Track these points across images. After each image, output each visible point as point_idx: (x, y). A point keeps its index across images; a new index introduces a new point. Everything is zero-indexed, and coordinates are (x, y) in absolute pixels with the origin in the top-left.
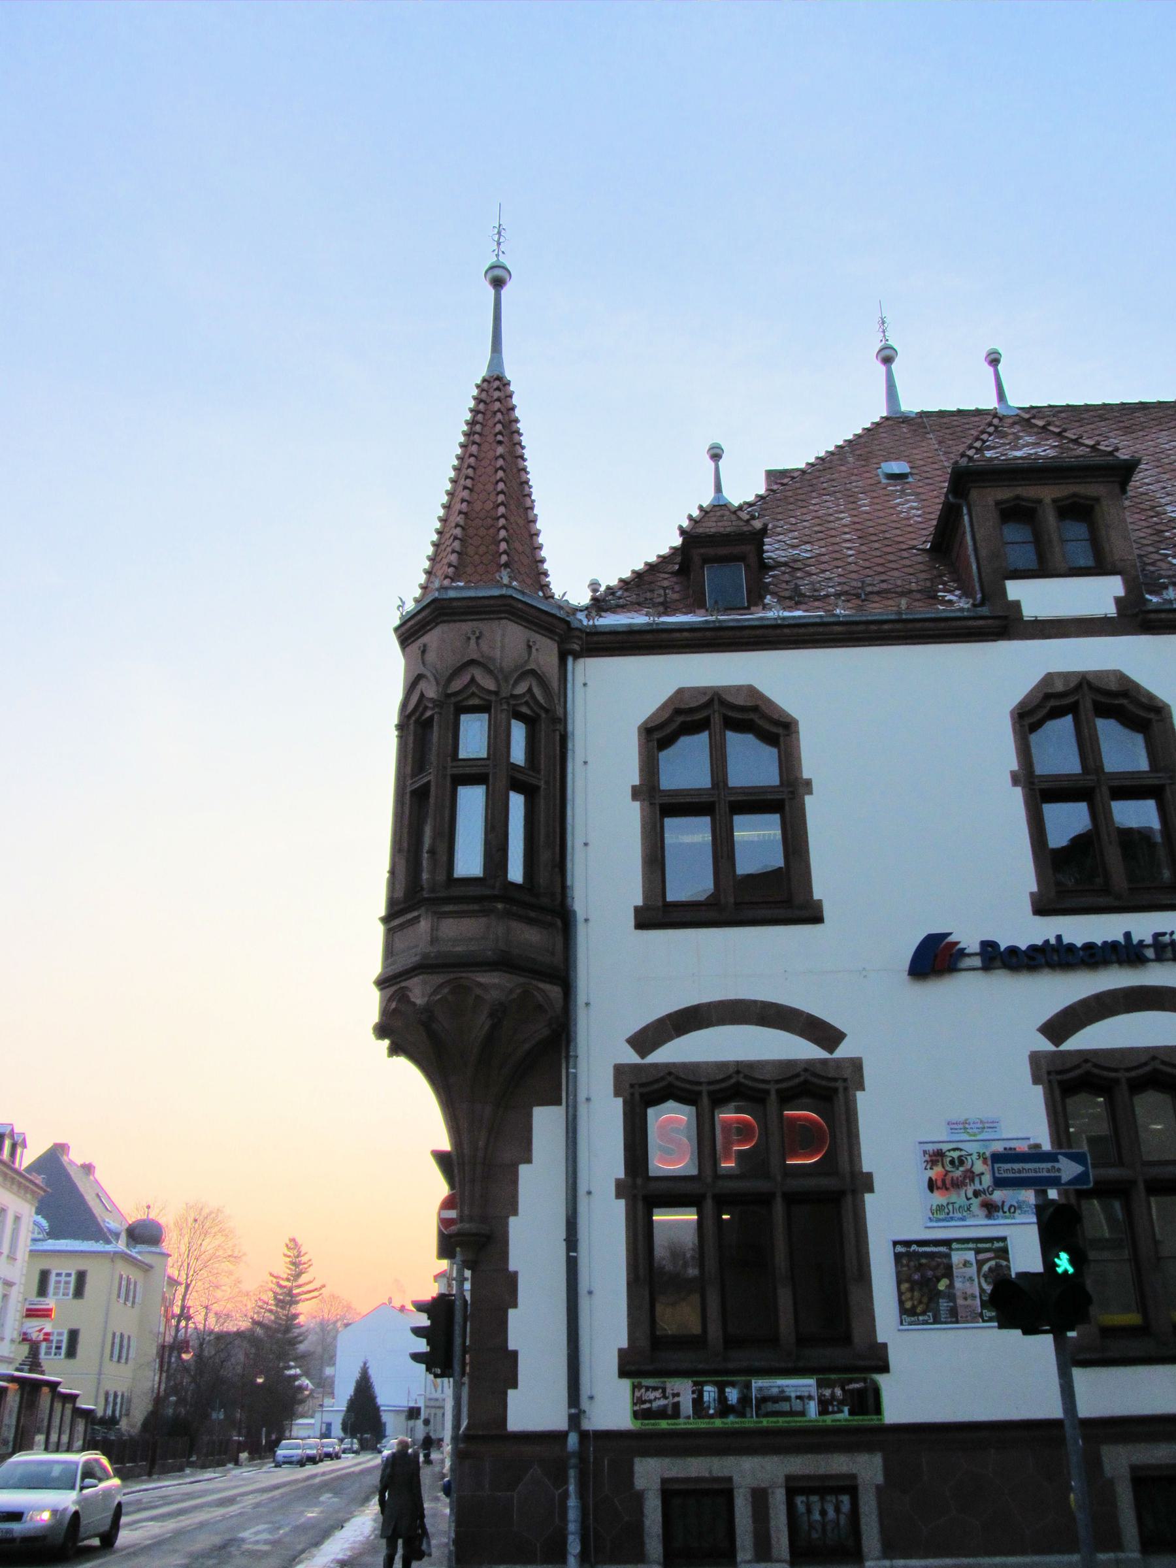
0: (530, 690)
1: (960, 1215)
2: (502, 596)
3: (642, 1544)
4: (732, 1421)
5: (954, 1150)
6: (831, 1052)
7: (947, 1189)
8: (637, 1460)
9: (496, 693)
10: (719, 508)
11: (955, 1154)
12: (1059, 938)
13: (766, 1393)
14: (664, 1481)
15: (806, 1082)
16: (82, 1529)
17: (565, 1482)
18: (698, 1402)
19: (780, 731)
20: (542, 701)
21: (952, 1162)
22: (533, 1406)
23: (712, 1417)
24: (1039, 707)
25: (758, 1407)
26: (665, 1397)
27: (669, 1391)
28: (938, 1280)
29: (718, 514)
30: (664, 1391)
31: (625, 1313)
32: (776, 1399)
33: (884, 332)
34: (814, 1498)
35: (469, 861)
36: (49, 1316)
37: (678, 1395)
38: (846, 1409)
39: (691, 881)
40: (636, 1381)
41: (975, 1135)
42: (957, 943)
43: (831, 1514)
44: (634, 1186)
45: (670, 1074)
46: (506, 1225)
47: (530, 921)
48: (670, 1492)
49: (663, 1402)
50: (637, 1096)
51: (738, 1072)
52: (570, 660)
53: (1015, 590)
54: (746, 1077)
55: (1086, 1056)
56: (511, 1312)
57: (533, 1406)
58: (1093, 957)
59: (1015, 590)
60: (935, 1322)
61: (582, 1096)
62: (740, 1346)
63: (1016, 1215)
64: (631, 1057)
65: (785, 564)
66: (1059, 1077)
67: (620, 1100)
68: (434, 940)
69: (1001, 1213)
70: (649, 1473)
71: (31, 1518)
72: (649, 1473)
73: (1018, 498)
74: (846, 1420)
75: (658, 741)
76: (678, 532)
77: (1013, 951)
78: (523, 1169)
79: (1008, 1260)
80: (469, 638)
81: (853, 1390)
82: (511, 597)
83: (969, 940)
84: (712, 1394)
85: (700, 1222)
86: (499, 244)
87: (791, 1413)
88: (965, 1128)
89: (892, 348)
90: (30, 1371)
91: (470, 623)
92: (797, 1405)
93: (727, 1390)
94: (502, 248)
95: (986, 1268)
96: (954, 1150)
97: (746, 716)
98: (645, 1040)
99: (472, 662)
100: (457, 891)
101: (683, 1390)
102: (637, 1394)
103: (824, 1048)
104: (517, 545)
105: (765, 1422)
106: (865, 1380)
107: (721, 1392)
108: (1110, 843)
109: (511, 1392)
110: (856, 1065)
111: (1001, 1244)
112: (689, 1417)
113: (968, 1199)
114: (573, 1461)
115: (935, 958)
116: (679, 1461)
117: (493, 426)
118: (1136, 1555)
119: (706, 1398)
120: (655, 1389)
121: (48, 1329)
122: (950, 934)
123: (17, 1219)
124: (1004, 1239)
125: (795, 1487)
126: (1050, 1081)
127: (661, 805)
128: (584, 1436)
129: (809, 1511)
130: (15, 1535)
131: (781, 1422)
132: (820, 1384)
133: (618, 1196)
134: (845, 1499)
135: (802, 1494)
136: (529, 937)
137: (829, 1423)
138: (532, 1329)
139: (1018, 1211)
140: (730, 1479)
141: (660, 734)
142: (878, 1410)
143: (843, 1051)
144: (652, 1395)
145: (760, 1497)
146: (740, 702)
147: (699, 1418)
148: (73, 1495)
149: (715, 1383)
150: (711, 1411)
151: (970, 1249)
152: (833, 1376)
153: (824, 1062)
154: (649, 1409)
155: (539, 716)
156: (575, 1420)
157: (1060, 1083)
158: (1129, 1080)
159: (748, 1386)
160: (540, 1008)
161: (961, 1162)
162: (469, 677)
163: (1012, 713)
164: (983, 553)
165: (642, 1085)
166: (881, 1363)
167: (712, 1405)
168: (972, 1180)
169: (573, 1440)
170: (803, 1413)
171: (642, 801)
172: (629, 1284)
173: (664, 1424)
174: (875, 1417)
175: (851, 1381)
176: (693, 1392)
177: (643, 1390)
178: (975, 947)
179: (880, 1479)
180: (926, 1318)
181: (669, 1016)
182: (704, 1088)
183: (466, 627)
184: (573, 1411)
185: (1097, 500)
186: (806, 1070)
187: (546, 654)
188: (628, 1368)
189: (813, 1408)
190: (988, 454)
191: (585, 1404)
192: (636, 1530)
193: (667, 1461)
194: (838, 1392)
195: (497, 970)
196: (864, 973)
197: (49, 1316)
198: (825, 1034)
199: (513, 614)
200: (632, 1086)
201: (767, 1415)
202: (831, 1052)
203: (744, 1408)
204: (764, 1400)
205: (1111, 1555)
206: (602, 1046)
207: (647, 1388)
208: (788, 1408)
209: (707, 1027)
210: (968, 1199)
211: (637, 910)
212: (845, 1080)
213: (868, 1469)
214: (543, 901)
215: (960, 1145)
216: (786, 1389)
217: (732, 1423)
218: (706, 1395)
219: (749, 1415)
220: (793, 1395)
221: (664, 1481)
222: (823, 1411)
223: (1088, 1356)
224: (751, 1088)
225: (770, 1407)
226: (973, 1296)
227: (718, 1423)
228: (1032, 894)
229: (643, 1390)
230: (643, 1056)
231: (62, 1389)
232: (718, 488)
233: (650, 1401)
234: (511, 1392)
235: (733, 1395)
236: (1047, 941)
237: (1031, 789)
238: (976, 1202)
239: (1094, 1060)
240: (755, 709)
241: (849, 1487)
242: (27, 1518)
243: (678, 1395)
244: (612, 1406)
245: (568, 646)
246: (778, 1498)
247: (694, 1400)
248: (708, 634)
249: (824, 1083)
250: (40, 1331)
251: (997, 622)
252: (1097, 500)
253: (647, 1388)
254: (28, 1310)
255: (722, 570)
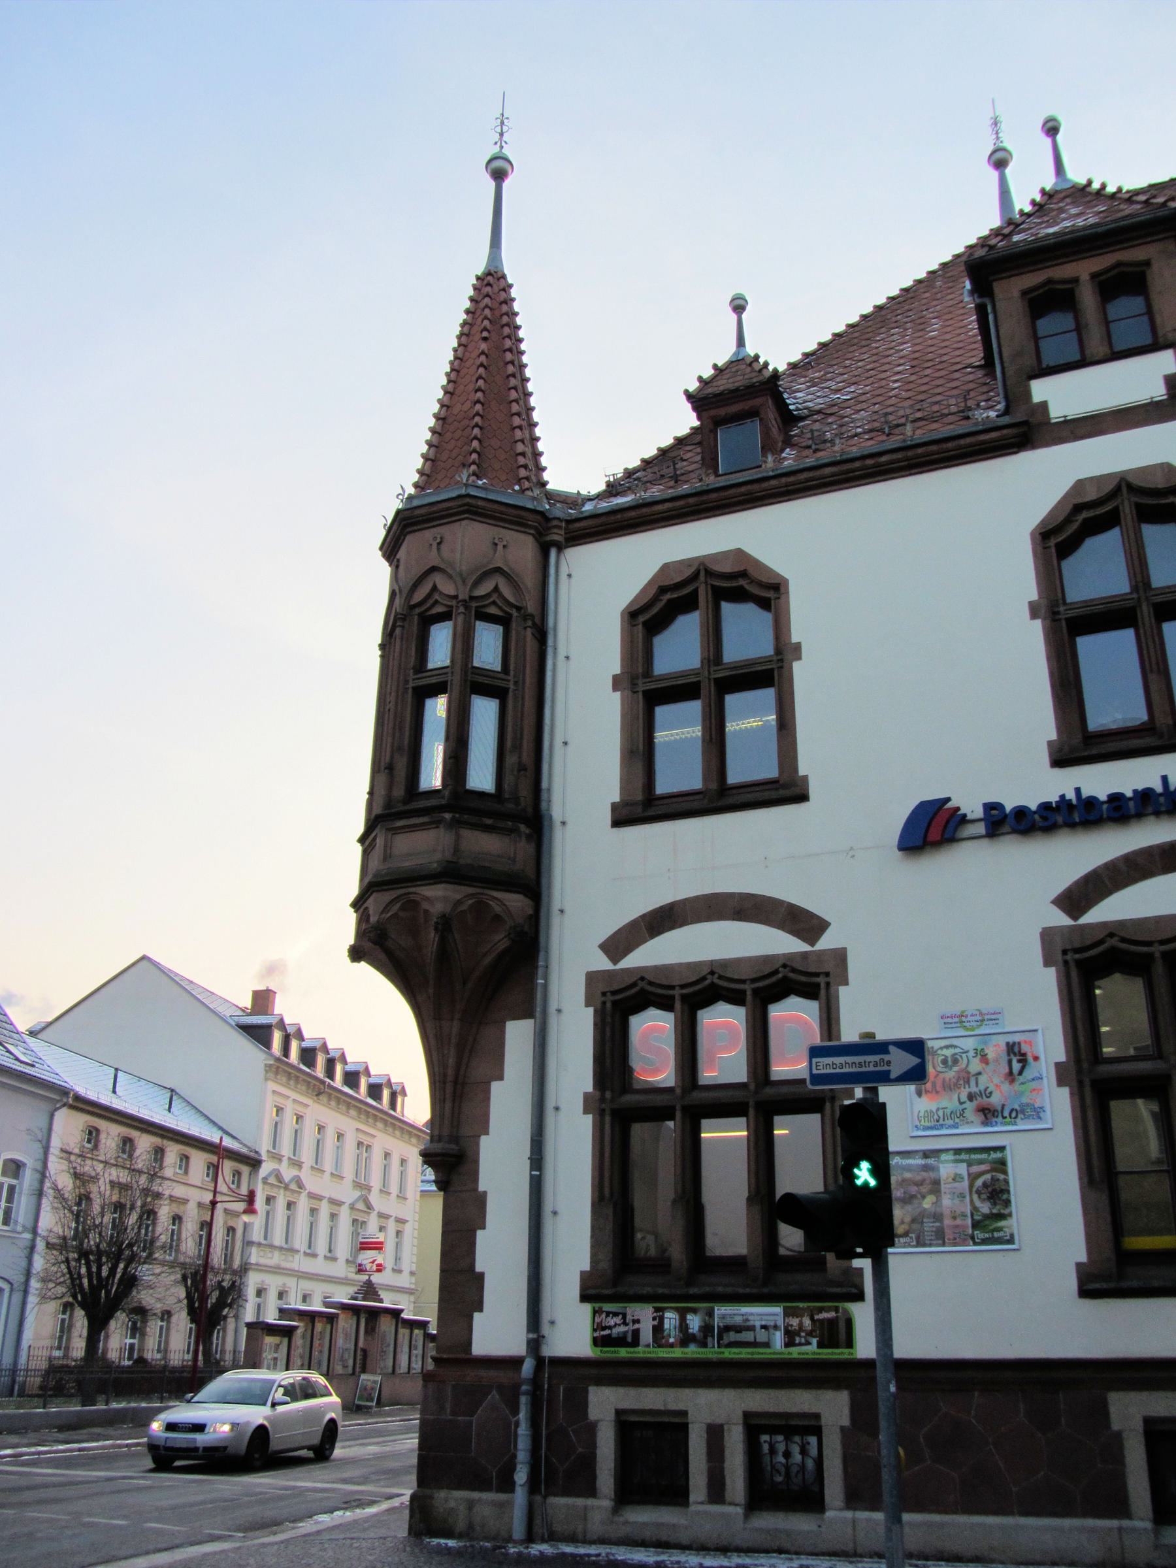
0: (496, 589)
1: (950, 1122)
2: (460, 497)
3: (593, 1477)
4: (692, 1351)
5: (947, 1047)
6: (813, 945)
7: (937, 1092)
8: (592, 1390)
9: (456, 597)
10: (743, 363)
11: (948, 1053)
12: (1078, 791)
13: (729, 1321)
14: (619, 1413)
15: (785, 978)
16: (271, 1444)
17: (515, 1411)
18: (658, 1330)
19: (771, 594)
20: (512, 599)
21: (945, 1062)
22: (497, 1332)
23: (672, 1346)
24: (1068, 520)
25: (720, 1338)
26: (625, 1323)
27: (629, 1318)
28: (924, 1197)
29: (734, 370)
30: (624, 1316)
31: (589, 1234)
32: (738, 1329)
33: (997, 133)
34: (780, 1438)
35: (433, 776)
36: (380, 1249)
37: (638, 1321)
38: (814, 1341)
39: (679, 772)
40: (597, 1305)
41: (972, 1029)
42: (958, 809)
43: (797, 1458)
44: (602, 1099)
45: (642, 979)
46: (478, 1144)
47: (487, 829)
48: (626, 1424)
49: (623, 1329)
50: (609, 1005)
51: (712, 973)
52: (553, 553)
53: (1041, 390)
54: (720, 977)
55: (1112, 930)
56: (480, 1234)
57: (497, 1332)
58: (1120, 810)
59: (1041, 390)
60: (919, 1244)
61: (553, 1006)
62: (832, 1323)
63: (1018, 1120)
64: (603, 963)
65: (819, 412)
66: (1077, 956)
67: (591, 1010)
68: (386, 857)
69: (1000, 1119)
70: (604, 1403)
71: (215, 1431)
72: (604, 1403)
73: (1049, 281)
74: (814, 1353)
75: (645, 624)
76: (684, 397)
77: (1021, 812)
78: (495, 1086)
79: (1005, 1172)
80: (496, 544)
81: (822, 1321)
82: (468, 496)
83: (972, 807)
84: (673, 1321)
85: (748, 1136)
86: (502, 134)
87: (754, 1344)
88: (962, 1022)
89: (1004, 149)
90: (364, 1299)
91: (432, 530)
92: (762, 1336)
93: (689, 1317)
94: (505, 138)
95: (979, 1182)
96: (947, 1047)
97: (734, 584)
98: (617, 946)
99: (498, 570)
100: (422, 804)
101: (644, 1315)
102: (598, 1320)
103: (804, 940)
104: (495, 443)
105: (729, 1354)
106: (836, 1309)
107: (683, 1319)
108: (1151, 671)
109: (476, 1315)
110: (840, 956)
111: (998, 1155)
112: (648, 1346)
113: (961, 1103)
114: (524, 1388)
115: (932, 829)
116: (632, 1392)
117: (491, 323)
118: (1148, 1525)
119: (666, 1326)
120: (615, 1314)
121: (380, 1261)
122: (949, 799)
123: (403, 1162)
124: (1002, 1149)
125: (754, 1426)
126: (1066, 963)
127: (647, 693)
128: (540, 1361)
129: (773, 1451)
130: (198, 1445)
131: (743, 1354)
132: (787, 1313)
133: (586, 1111)
134: (813, 1440)
135: (766, 1433)
136: (485, 845)
137: (795, 1356)
138: (499, 1251)
139: (1021, 1116)
140: (684, 1413)
141: (650, 616)
142: (850, 1343)
143: (825, 943)
144: (611, 1321)
145: (715, 1434)
146: (727, 568)
147: (660, 1346)
148: (266, 1410)
149: (677, 1309)
150: (672, 1340)
151: (962, 1161)
152: (801, 1305)
153: (805, 955)
154: (610, 1335)
155: (511, 615)
156: (535, 1345)
157: (1078, 963)
158: (1164, 955)
159: (710, 1314)
160: (497, 918)
161: (955, 1062)
162: (430, 585)
163: (1032, 534)
164: (1005, 355)
165: (614, 993)
166: (854, 1291)
167: (673, 1333)
168: (968, 1082)
169: (528, 1367)
170: (767, 1345)
171: (622, 690)
172: (593, 1205)
173: (623, 1353)
174: (846, 1351)
175: (821, 1310)
176: (654, 1319)
177: (604, 1315)
178: (979, 813)
179: (846, 1421)
180: (907, 1240)
181: (644, 916)
182: (677, 992)
183: (428, 535)
184: (531, 1336)
185: (1147, 263)
186: (784, 966)
187: (521, 550)
188: (592, 1292)
189: (778, 1338)
190: (1016, 238)
191: (546, 1329)
192: (588, 1463)
193: (621, 1391)
194: (807, 1322)
195: (441, 882)
196: (851, 853)
197: (380, 1249)
198: (805, 924)
199: (476, 513)
200: (604, 994)
201: (731, 1345)
202: (813, 945)
203: (705, 1337)
204: (728, 1328)
205: (1115, 1523)
206: (574, 956)
207: (608, 1314)
208: (752, 1339)
209: (681, 925)
210: (961, 1103)
211: (614, 807)
212: (827, 974)
213: (833, 1408)
214: (521, 808)
215: (955, 1042)
216: (751, 1318)
217: (693, 1353)
218: (666, 1321)
219: (710, 1345)
220: (758, 1324)
221: (619, 1413)
222: (789, 1343)
223: (1097, 1286)
224: (728, 989)
225: (733, 1336)
226: (964, 1215)
227: (677, 1353)
228: (1050, 743)
229: (604, 1315)
230: (615, 963)
231: (404, 1315)
232: (741, 342)
233: (610, 1328)
234: (476, 1315)
235: (694, 1323)
236: (1063, 797)
237: (1054, 620)
238: (970, 1106)
239: (1122, 934)
240: (743, 574)
241: (810, 1426)
242: (208, 1429)
243: (638, 1321)
244: (572, 1333)
245: (548, 538)
246: (735, 1440)
247: (654, 1327)
248: (691, 500)
249: (803, 979)
250: (373, 1262)
251: (1014, 431)
252: (1147, 263)
253: (608, 1314)
254: (362, 1243)
255: (754, 431)
